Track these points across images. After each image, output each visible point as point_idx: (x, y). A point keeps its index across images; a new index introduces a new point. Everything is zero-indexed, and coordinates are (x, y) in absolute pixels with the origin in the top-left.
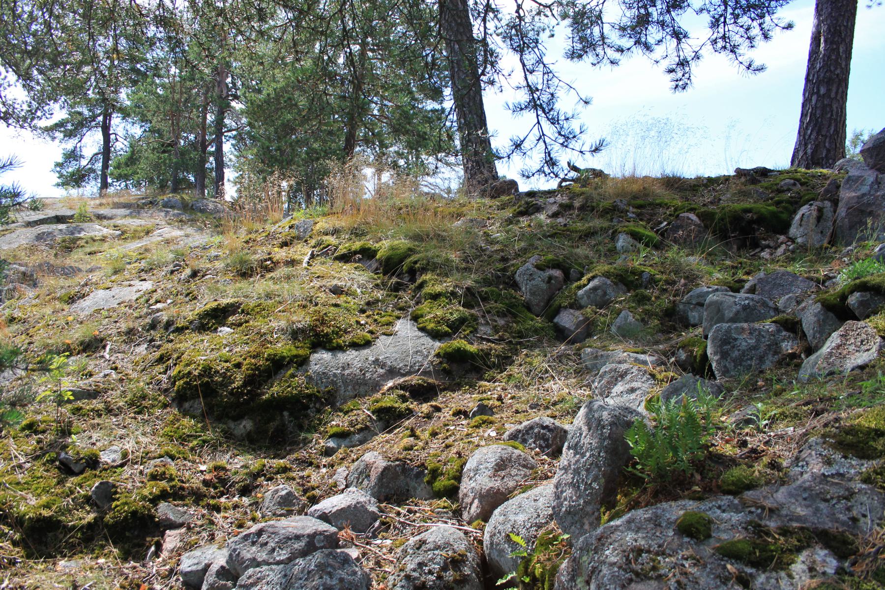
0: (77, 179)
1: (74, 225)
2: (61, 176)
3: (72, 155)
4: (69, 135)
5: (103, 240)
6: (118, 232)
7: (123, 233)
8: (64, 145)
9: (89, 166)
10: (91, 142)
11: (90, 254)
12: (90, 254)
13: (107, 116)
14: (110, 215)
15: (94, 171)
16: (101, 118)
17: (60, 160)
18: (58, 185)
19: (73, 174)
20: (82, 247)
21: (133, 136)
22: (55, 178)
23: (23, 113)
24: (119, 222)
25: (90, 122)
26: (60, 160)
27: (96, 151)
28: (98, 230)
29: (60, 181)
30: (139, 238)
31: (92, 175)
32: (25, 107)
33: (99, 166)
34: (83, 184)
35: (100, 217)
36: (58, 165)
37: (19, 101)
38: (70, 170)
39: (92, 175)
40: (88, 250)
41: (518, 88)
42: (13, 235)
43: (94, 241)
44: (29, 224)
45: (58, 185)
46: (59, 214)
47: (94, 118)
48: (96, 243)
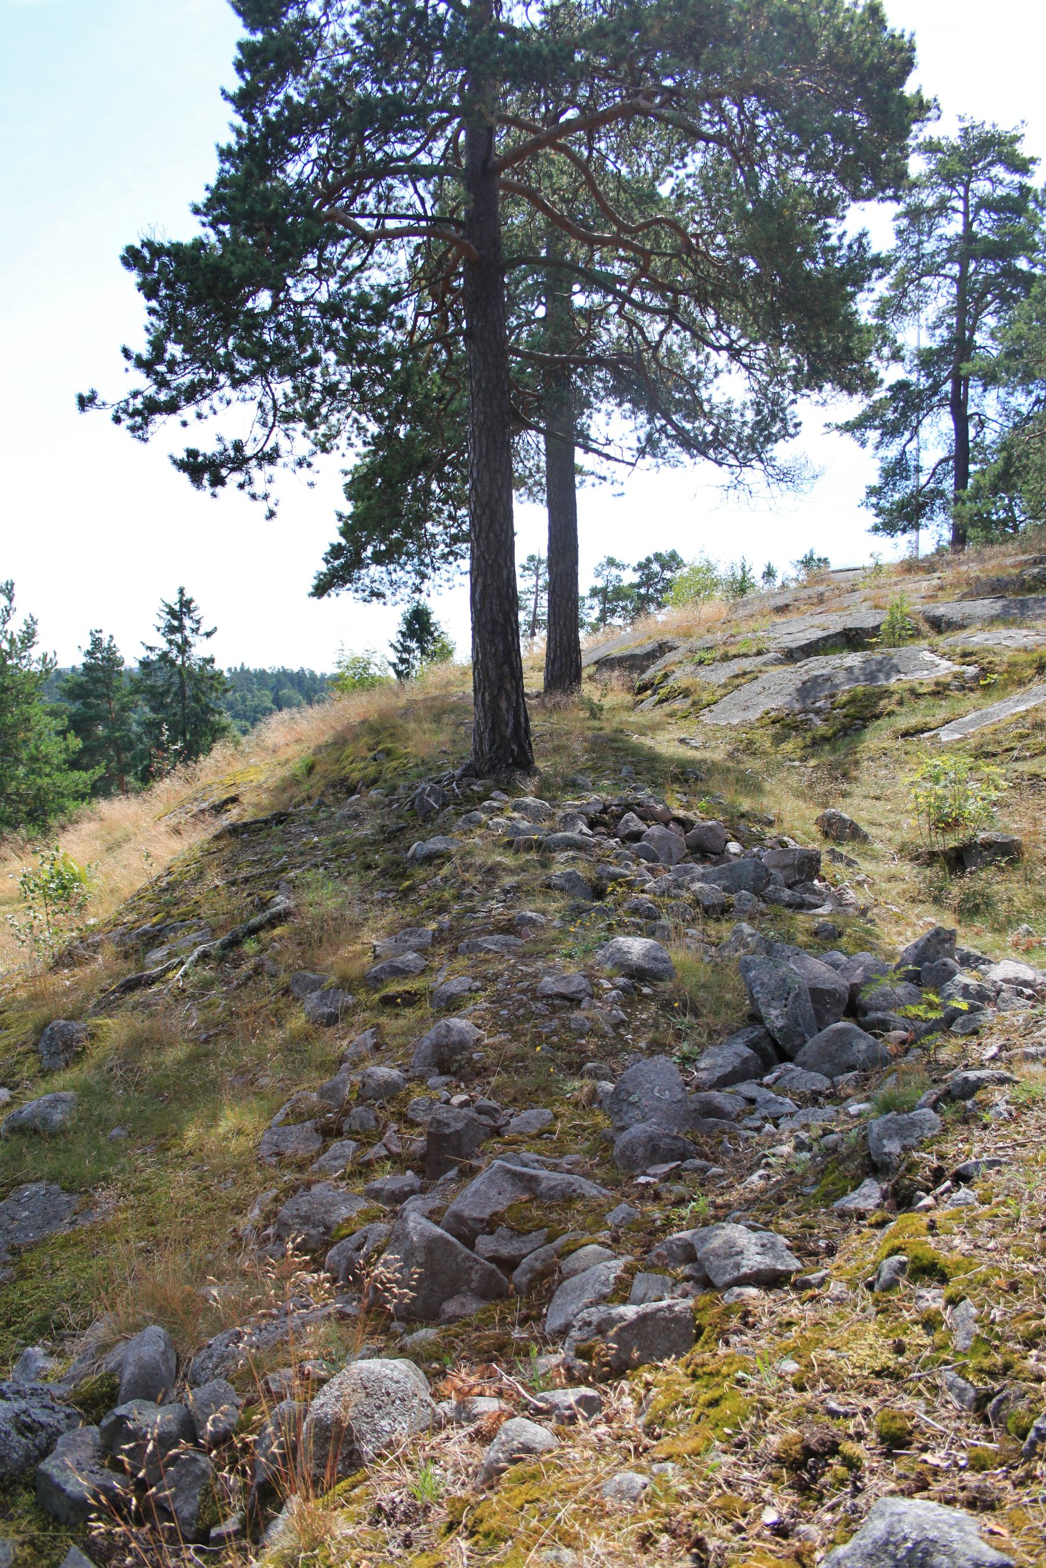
0: (904, 516)
1: (877, 655)
2: (880, 512)
3: (897, 470)
4: (891, 431)
5: (940, 691)
6: (972, 670)
7: (984, 671)
8: (883, 452)
9: (931, 486)
10: (934, 437)
11: (906, 734)
12: (906, 734)
13: (960, 381)
14: (957, 617)
15: (941, 494)
16: (948, 387)
17: (876, 481)
18: (876, 529)
19: (902, 505)
20: (891, 714)
21: (1018, 413)
22: (870, 518)
23: (747, 431)
24: (977, 638)
25: (929, 398)
26: (876, 481)
27: (944, 454)
28: (929, 664)
29: (879, 521)
30: (1021, 683)
31: (938, 502)
32: (750, 416)
33: (948, 484)
34: (923, 521)
35: (939, 625)
36: (873, 491)
37: (737, 405)
38: (897, 497)
39: (938, 502)
40: (903, 723)
41: (220, 439)
42: (756, 686)
43: (918, 696)
44: (791, 656)
45: (876, 529)
46: (851, 624)
47: (935, 389)
48: (922, 703)
